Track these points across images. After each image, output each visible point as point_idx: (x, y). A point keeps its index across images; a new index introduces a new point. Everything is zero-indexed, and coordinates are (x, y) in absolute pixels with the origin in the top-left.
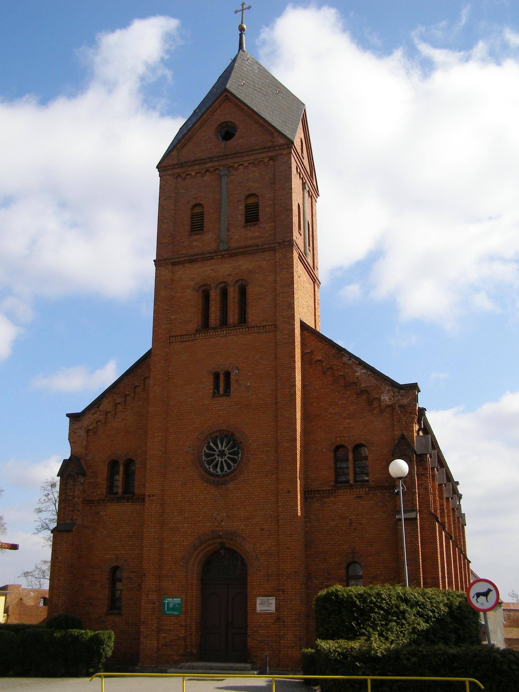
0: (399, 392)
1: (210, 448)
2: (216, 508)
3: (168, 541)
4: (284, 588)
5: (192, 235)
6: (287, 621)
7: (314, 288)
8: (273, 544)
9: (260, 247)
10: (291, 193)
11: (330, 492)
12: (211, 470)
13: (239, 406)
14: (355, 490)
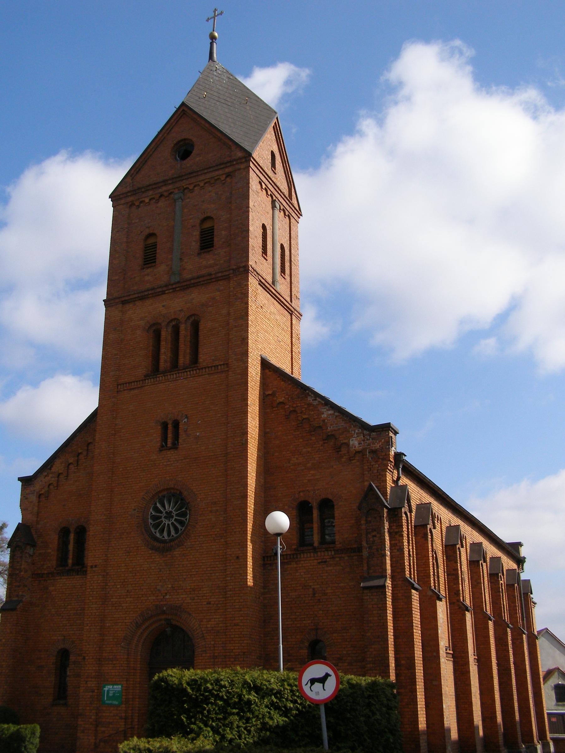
0: (370, 435)
1: (156, 510)
3: (110, 619)
5: (144, 268)
7: (291, 320)
8: (220, 620)
9: (213, 276)
10: (248, 212)
11: (292, 556)
12: (158, 535)
13: (187, 460)
14: (319, 553)
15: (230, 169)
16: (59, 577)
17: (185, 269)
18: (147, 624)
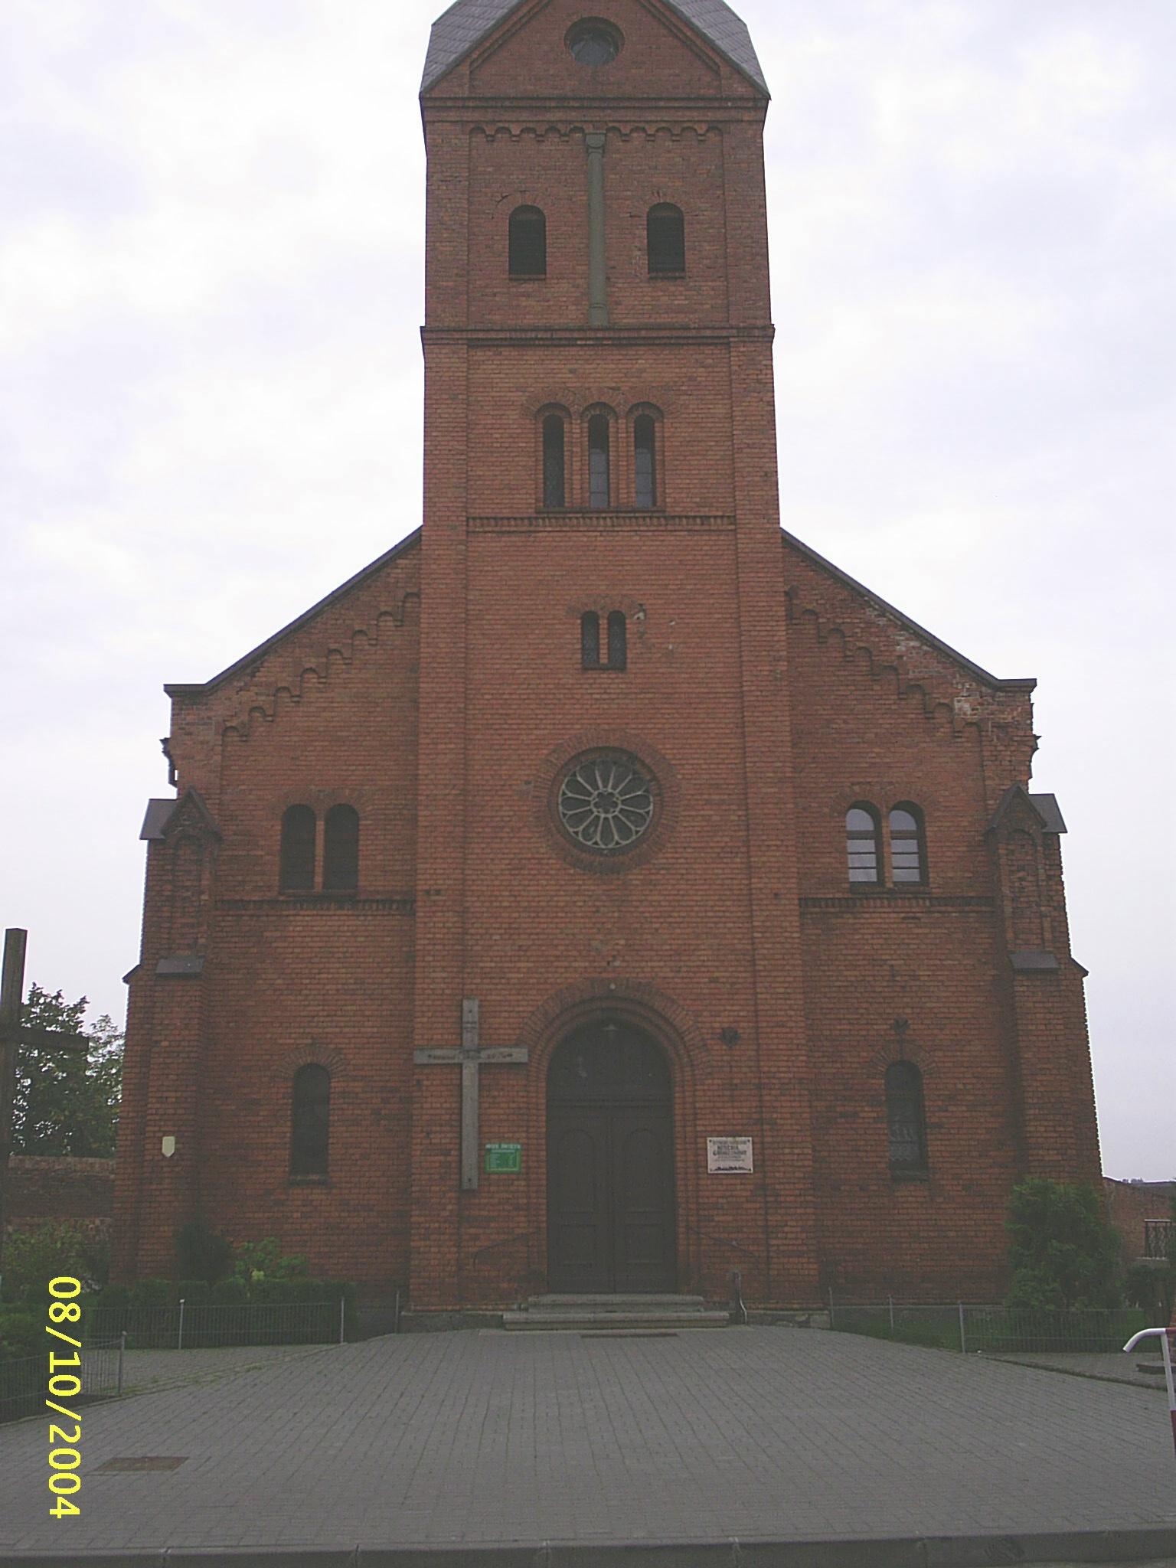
0: (993, 697)
1: (574, 785)
9: (693, 333)
15: (720, 115)
17: (618, 303)
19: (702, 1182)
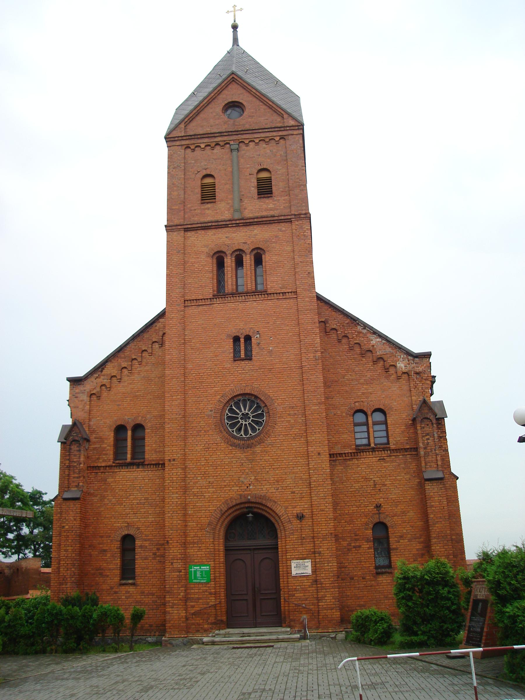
0: (413, 360)
1: (231, 410)
2: (243, 471)
3: (192, 507)
4: (320, 550)
6: (324, 583)
9: (276, 218)
12: (235, 433)
16: (119, 470)
18: (230, 511)
19: (289, 580)
